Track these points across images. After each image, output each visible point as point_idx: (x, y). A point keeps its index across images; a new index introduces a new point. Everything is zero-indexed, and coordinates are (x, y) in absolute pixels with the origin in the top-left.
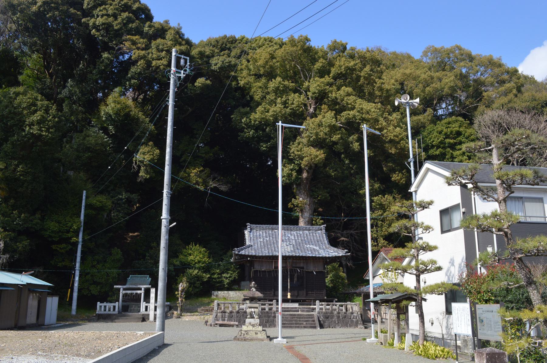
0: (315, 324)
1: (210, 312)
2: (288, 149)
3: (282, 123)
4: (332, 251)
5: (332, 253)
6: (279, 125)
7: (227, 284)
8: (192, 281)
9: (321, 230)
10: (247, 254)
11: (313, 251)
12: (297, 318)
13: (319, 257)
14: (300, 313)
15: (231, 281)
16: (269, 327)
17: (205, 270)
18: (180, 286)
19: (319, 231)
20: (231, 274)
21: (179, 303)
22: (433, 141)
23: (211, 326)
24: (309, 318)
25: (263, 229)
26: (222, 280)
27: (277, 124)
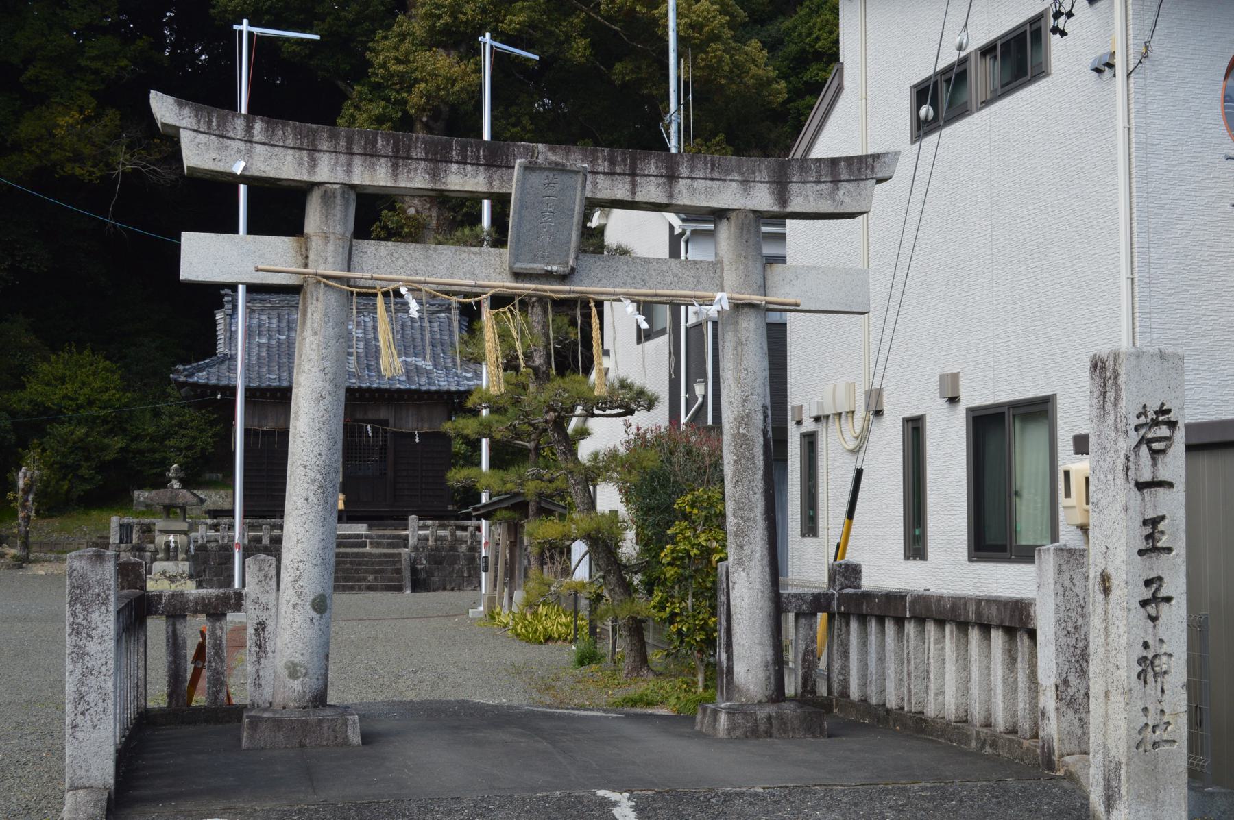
0: (400, 579)
2: (368, 55)
3: (251, 24)
4: (469, 375)
5: (468, 379)
6: (241, 32)
8: (70, 461)
10: (213, 381)
11: (414, 375)
12: (351, 563)
13: (428, 392)
14: (368, 549)
17: (110, 426)
18: (21, 474)
20: (194, 439)
22: (818, 39)
24: (387, 563)
25: (272, 308)
27: (236, 27)
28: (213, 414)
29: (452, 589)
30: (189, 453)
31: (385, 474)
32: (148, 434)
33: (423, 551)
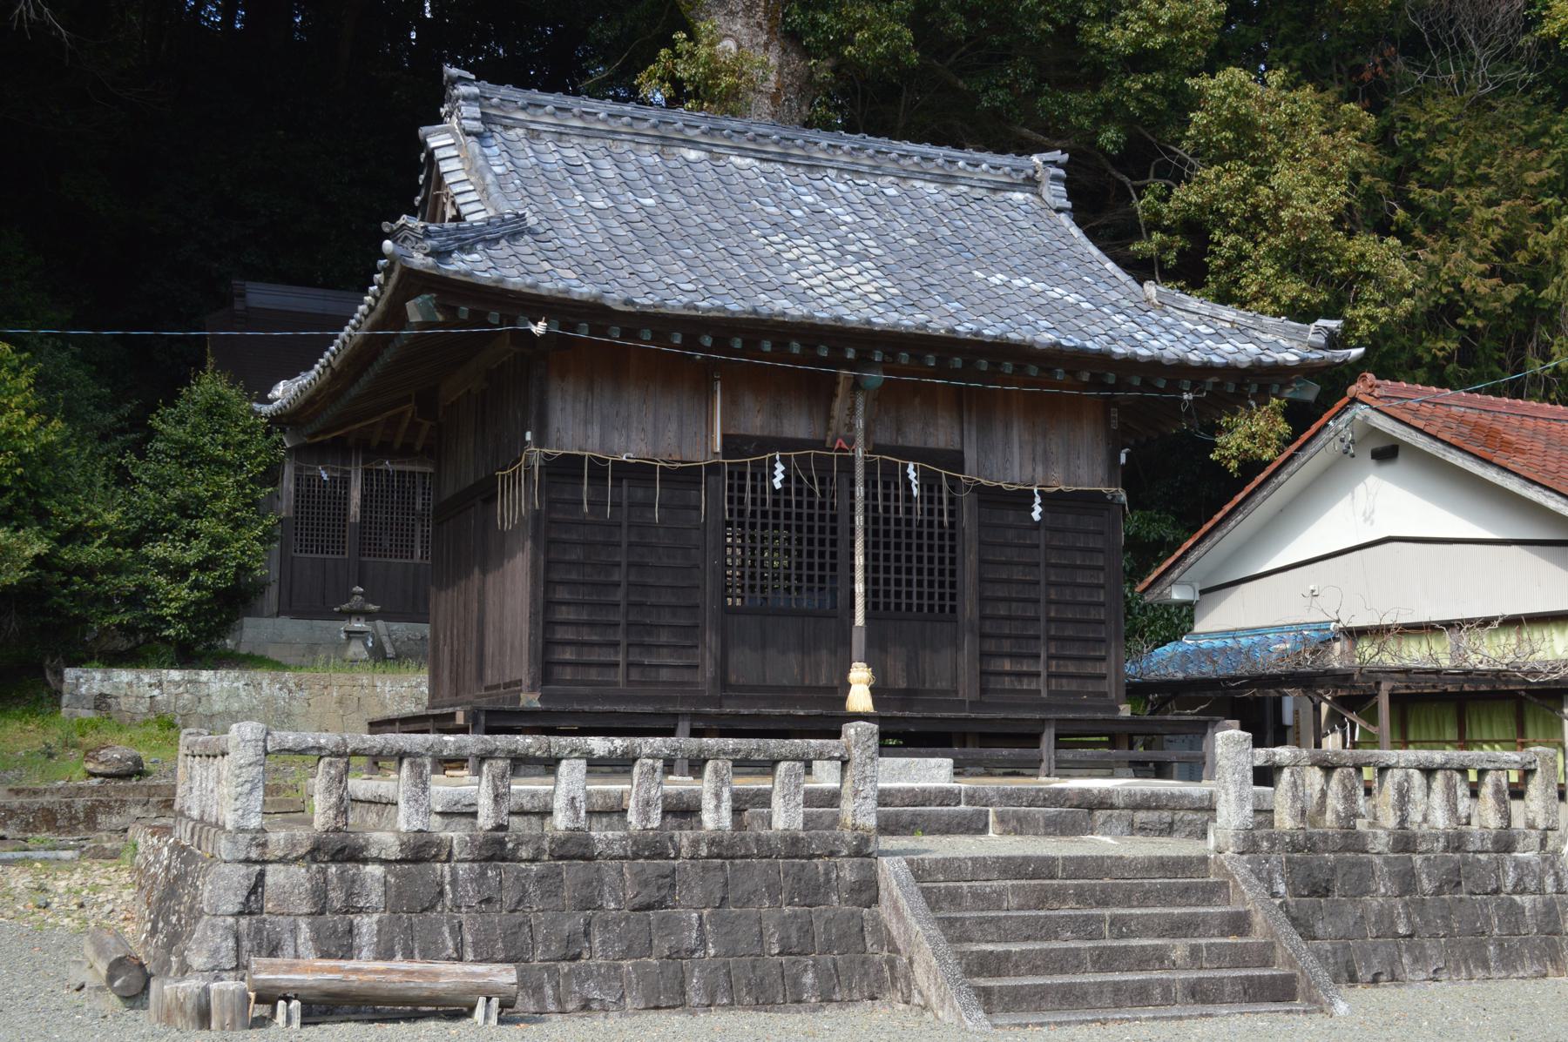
1: (71, 830)
7: (179, 617)
9: (1031, 183)
15: (218, 593)
16: (827, 999)
19: (1018, 196)
20: (217, 543)
23: (203, 1017)
26: (144, 589)
28: (263, 486)
29: (1375, 980)
30: (208, 579)
31: (953, 609)
32: (105, 527)
33: (1271, 850)
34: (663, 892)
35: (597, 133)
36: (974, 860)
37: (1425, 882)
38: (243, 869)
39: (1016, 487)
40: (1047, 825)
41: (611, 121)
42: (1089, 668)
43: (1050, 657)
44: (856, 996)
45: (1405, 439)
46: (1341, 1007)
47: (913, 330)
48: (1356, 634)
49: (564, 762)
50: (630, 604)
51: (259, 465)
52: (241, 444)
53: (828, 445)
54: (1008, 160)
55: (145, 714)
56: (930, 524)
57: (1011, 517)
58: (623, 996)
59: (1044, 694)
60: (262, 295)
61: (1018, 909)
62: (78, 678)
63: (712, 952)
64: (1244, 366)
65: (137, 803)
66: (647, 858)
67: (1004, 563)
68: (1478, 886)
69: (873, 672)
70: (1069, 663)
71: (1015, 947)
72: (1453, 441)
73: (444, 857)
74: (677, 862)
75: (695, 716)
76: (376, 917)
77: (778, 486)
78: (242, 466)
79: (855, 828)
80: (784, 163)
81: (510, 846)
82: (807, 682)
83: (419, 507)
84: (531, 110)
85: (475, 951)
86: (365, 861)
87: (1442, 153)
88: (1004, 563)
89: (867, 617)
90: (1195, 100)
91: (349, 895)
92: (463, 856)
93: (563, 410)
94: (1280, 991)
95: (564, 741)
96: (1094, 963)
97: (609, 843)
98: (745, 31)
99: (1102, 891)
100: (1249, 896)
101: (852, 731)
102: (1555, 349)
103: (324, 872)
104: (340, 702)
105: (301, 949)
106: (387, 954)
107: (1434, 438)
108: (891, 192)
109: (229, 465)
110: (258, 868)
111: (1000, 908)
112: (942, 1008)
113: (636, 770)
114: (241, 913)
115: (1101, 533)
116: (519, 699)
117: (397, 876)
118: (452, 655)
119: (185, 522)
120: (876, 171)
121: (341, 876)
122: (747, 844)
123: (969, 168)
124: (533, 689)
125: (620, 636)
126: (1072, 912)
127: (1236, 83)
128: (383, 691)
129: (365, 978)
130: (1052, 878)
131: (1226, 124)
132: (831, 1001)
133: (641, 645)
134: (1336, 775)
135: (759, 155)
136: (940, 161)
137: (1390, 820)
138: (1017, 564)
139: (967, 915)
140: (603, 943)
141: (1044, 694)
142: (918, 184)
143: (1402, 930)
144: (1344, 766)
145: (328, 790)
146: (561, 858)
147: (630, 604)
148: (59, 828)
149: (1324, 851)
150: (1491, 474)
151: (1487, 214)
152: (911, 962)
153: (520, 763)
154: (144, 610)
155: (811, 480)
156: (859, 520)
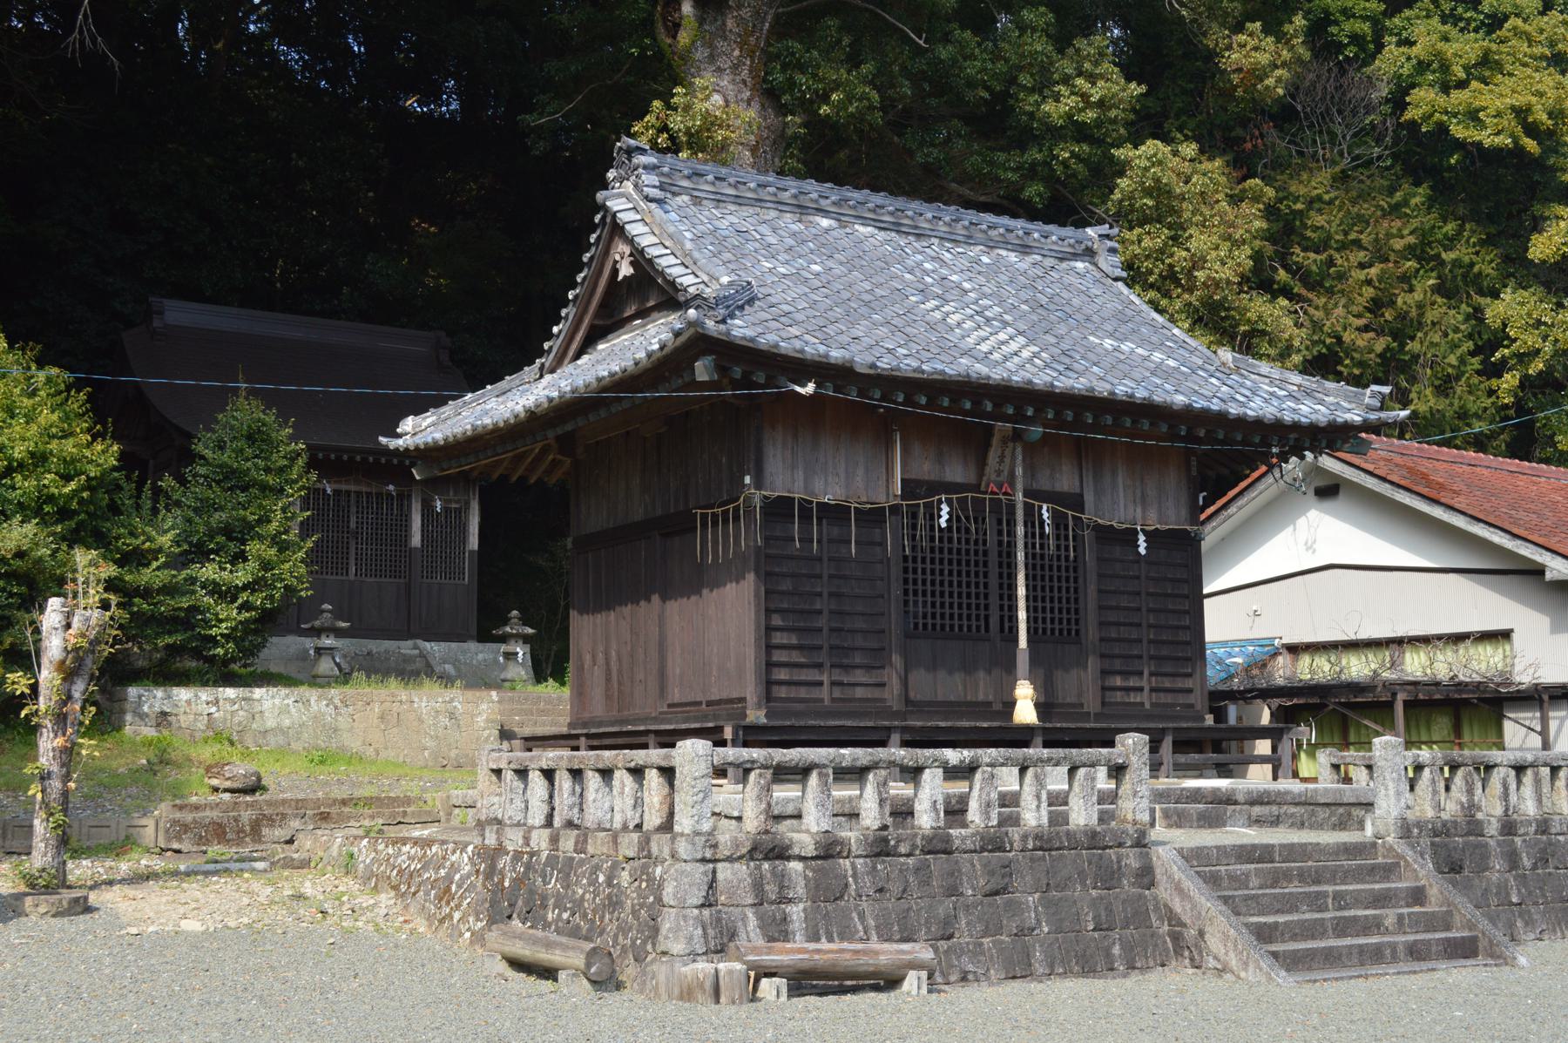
1: (239, 842)
9: (1089, 254)
20: (266, 566)
21: (44, 777)
31: (1077, 632)
34: (1006, 880)
35: (747, 202)
36: (1218, 848)
37: (1525, 859)
38: (701, 868)
39: (1124, 526)
40: (1199, 820)
41: (760, 190)
42: (1181, 683)
43: (1151, 674)
44: (1151, 964)
45: (1355, 480)
46: (1522, 960)
47: (1021, 385)
48: (1294, 649)
49: (927, 771)
50: (832, 630)
51: (300, 489)
52: (281, 470)
53: (983, 489)
54: (1068, 231)
55: (204, 731)
56: (1059, 557)
57: (1117, 551)
58: (988, 969)
59: (1147, 706)
60: (178, 314)
61: (1260, 888)
62: (140, 697)
63: (1046, 929)
64: (1323, 425)
65: (296, 816)
66: (990, 851)
67: (1114, 592)
68: (1560, 862)
69: (1035, 689)
70: (1165, 679)
71: (1281, 919)
72: (1402, 483)
73: (845, 854)
74: (1011, 855)
75: (904, 729)
76: (801, 906)
77: (944, 525)
78: (282, 490)
79: (1135, 823)
80: (898, 232)
81: (892, 843)
82: (969, 698)
83: (353, 525)
84: (695, 178)
85: (878, 933)
86: (789, 858)
87: (1319, 220)
88: (1114, 592)
89: (1029, 641)
90: (1121, 169)
91: (782, 887)
92: (859, 853)
93: (774, 456)
94: (1464, 950)
95: (928, 752)
96: (1334, 930)
97: (964, 839)
98: (731, 87)
99: (1316, 872)
100: (1422, 873)
101: (1131, 741)
102: (1413, 395)
103: (758, 868)
104: (382, 718)
105: (752, 935)
106: (815, 938)
107: (1384, 479)
108: (985, 259)
109: (271, 489)
110: (711, 866)
111: (1247, 888)
112: (1246, 970)
113: (978, 776)
114: (703, 906)
115: (1186, 566)
116: (745, 716)
117: (814, 871)
118: (608, 679)
119: (232, 545)
120: (969, 240)
121: (773, 871)
122: (1060, 838)
123: (1043, 240)
124: (759, 707)
125: (822, 657)
126: (1294, 890)
127: (1160, 155)
128: (420, 707)
129: (825, 957)
130: (1272, 862)
131: (1148, 192)
132: (1134, 968)
133: (840, 666)
134: (1460, 773)
135: (878, 224)
136: (1020, 233)
137: (1499, 810)
138: (1123, 593)
139: (1236, 893)
140: (968, 924)
141: (1147, 706)
142: (1004, 253)
143: (1515, 900)
144: (1467, 765)
145: (759, 798)
146: (929, 852)
147: (832, 630)
148: (228, 841)
149: (1456, 835)
150: (1438, 512)
151: (1361, 275)
152: (1201, 934)
153: (782, 773)
154: (193, 630)
155: (967, 518)
156: (1021, 556)
